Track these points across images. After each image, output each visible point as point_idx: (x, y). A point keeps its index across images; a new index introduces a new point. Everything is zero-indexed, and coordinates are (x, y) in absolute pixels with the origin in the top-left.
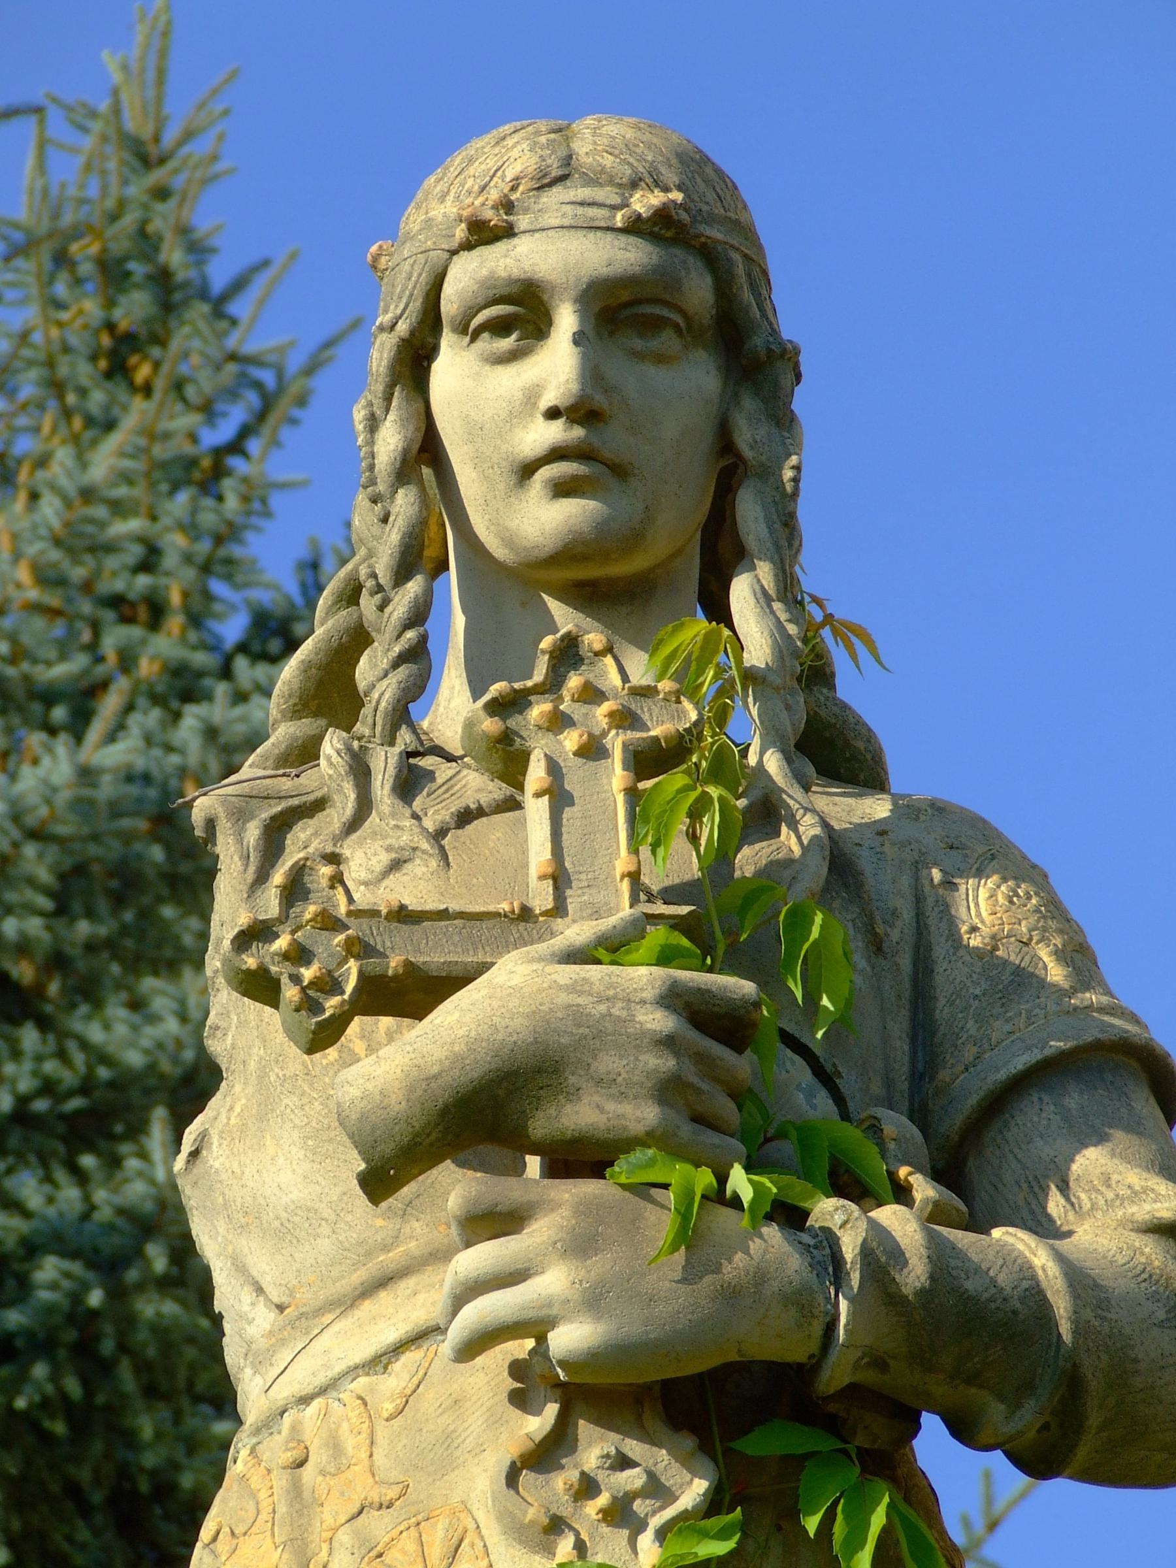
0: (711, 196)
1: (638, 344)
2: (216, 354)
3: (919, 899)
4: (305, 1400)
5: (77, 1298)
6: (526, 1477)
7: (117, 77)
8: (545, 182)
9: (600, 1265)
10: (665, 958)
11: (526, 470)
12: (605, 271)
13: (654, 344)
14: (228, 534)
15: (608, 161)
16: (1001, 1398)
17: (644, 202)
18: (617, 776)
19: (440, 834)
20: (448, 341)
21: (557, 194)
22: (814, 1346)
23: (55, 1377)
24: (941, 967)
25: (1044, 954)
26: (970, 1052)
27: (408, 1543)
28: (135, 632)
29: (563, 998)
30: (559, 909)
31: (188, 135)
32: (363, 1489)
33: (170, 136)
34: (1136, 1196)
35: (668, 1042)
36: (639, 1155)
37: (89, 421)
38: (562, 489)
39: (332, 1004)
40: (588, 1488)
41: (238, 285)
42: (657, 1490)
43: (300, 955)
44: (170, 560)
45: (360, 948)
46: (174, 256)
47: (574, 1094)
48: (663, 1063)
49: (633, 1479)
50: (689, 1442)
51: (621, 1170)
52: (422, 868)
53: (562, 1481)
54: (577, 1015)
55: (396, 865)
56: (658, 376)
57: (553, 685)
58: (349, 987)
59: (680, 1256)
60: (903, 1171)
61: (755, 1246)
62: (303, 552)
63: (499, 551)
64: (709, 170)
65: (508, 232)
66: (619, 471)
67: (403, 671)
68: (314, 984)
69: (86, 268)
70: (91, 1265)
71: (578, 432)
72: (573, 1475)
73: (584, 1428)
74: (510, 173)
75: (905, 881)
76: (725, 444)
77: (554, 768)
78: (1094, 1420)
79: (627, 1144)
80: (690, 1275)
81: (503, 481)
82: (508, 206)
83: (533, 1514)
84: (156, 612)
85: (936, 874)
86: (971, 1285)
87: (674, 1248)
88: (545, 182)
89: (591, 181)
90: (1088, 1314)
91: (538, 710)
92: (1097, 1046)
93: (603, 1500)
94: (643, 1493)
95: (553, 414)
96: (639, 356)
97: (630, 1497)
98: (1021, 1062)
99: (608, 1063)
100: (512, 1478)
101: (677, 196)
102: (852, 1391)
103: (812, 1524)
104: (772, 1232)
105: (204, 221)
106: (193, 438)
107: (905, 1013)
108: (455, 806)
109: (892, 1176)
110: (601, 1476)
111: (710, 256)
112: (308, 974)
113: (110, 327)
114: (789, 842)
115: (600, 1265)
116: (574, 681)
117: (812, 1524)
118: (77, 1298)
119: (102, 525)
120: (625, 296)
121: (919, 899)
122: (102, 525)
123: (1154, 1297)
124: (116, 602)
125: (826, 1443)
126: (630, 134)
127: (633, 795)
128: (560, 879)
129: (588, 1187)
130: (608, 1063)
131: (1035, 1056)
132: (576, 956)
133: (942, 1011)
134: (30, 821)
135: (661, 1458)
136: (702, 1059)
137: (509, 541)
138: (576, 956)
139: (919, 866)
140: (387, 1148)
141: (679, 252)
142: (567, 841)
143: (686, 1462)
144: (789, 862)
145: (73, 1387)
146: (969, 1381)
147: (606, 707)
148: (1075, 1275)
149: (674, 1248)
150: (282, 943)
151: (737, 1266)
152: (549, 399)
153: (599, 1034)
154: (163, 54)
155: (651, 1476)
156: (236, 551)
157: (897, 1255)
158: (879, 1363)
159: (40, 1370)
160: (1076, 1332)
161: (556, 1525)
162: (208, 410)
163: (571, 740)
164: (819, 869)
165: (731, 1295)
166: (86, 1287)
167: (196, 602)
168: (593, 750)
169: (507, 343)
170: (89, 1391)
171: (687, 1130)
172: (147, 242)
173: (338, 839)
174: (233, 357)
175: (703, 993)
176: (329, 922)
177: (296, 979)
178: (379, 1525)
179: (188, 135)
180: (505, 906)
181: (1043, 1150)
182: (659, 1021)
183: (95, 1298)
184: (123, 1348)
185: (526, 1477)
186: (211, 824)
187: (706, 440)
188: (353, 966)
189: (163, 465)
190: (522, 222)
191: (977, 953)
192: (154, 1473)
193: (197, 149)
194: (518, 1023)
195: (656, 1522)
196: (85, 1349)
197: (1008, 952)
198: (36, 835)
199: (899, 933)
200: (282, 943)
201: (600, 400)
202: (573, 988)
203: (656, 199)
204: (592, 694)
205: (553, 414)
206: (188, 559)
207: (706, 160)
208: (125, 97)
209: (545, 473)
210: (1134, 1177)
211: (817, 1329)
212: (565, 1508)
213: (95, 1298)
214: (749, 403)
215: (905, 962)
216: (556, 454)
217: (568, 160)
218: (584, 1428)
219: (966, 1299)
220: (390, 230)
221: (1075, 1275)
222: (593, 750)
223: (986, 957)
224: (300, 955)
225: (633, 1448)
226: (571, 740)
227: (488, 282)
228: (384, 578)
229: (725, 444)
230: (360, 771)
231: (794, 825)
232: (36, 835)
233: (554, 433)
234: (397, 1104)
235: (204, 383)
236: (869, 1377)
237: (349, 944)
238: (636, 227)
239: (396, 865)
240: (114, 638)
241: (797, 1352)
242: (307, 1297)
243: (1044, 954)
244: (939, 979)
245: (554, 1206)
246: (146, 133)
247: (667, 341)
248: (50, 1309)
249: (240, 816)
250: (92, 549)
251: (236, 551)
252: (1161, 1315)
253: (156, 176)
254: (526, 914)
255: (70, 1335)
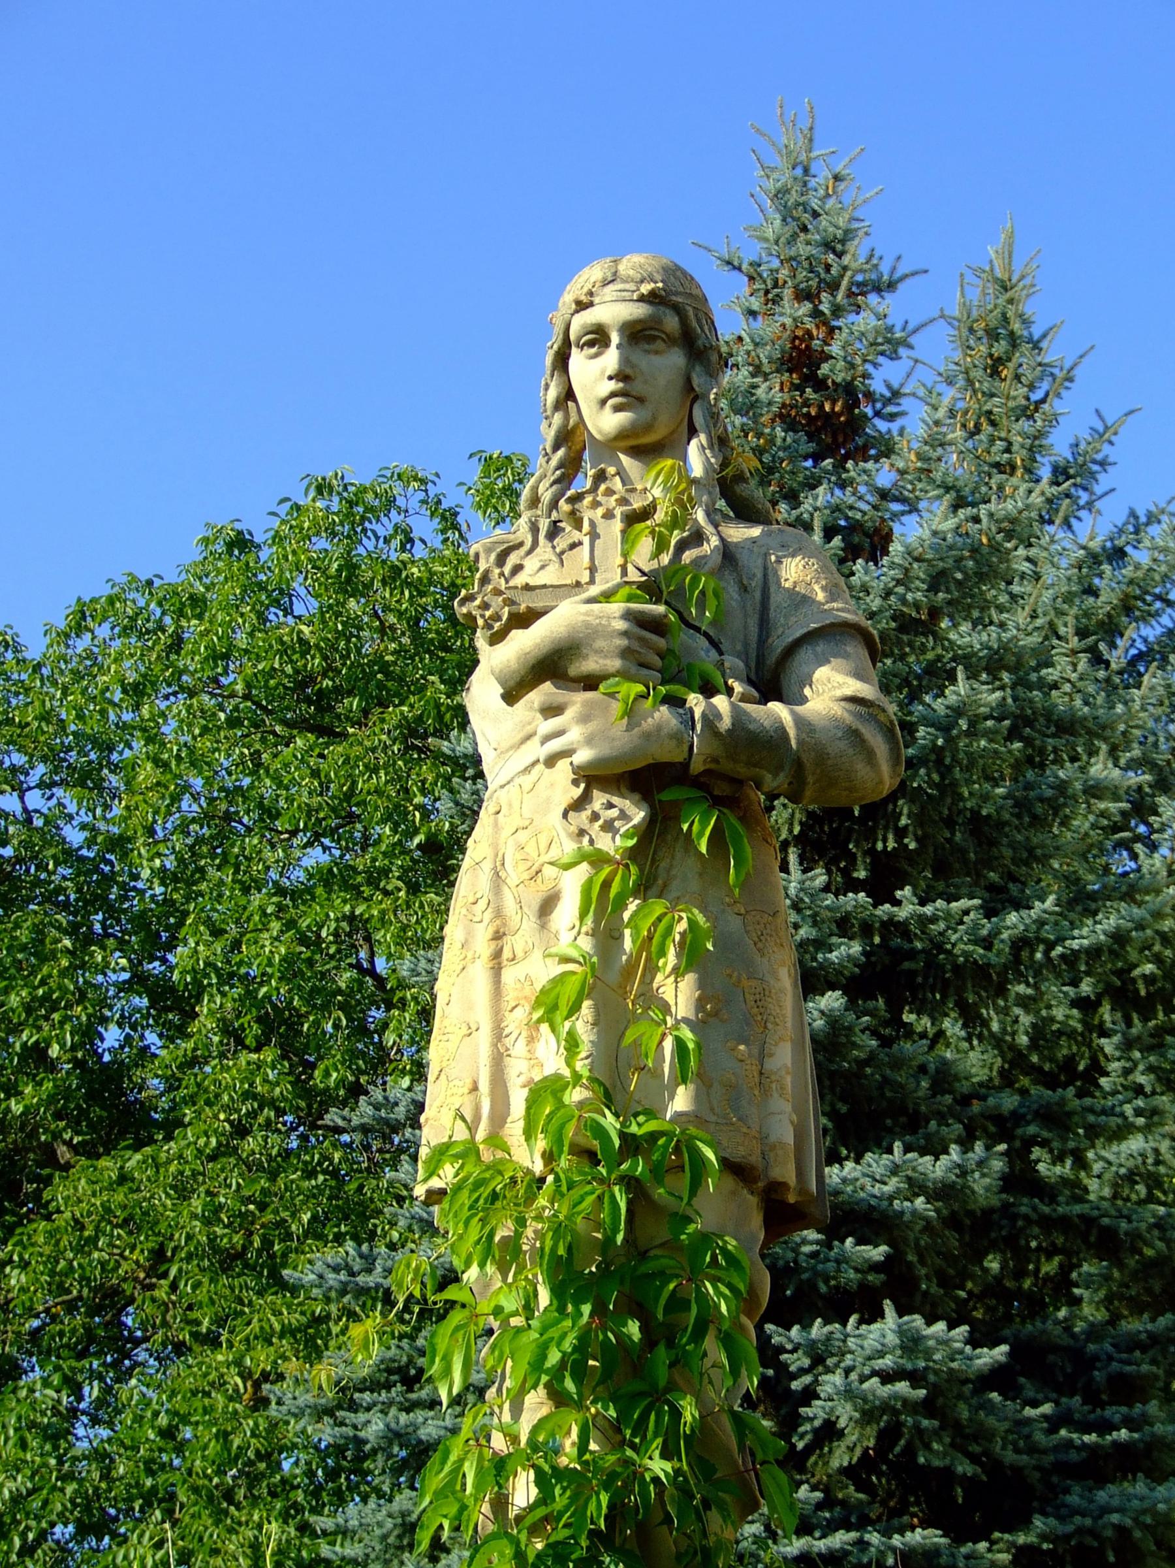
0: (677, 284)
1: (647, 347)
2: (1033, 364)
3: (765, 568)
4: (502, 787)
5: (934, 742)
6: (571, 814)
7: (993, 256)
8: (606, 283)
9: (592, 726)
10: (630, 599)
11: (603, 402)
12: (629, 318)
13: (652, 347)
14: (1040, 435)
15: (631, 272)
16: (769, 772)
17: (645, 288)
18: (617, 525)
19: (563, 553)
20: (574, 351)
21: (611, 287)
22: (686, 755)
23: (928, 775)
24: (773, 595)
25: (817, 587)
26: (780, 631)
27: (533, 842)
28: (1004, 476)
29: (582, 618)
30: (592, 581)
31: (1022, 277)
32: (518, 822)
33: (1014, 280)
34: (840, 686)
35: (625, 634)
36: (612, 681)
37: (984, 393)
38: (617, 409)
39: (497, 626)
40: (595, 817)
41: (1044, 336)
42: (623, 816)
43: (485, 606)
44: (1015, 448)
45: (510, 602)
46: (1016, 326)
47: (586, 657)
48: (623, 642)
49: (614, 813)
50: (637, 797)
51: (602, 688)
52: (553, 567)
53: (586, 814)
54: (587, 625)
55: (542, 567)
56: (656, 360)
57: (594, 489)
58: (505, 618)
59: (625, 721)
60: (730, 681)
61: (657, 715)
62: (1073, 441)
63: (598, 436)
64: (679, 273)
65: (591, 304)
66: (641, 400)
67: (555, 487)
68: (490, 618)
69: (980, 333)
70: (938, 729)
71: (621, 385)
72: (589, 812)
73: (596, 793)
74: (592, 280)
75: (760, 562)
76: (688, 386)
77: (592, 524)
78: (810, 780)
79: (604, 677)
80: (630, 727)
81: (595, 407)
82: (591, 294)
83: (573, 829)
84: (1013, 468)
85: (773, 558)
86: (751, 727)
87: (622, 718)
88: (606, 283)
89: (624, 281)
90: (804, 736)
91: (588, 499)
92: (832, 625)
93: (601, 822)
94: (618, 818)
95: (610, 378)
96: (648, 352)
97: (613, 820)
98: (798, 634)
99: (600, 644)
100: (565, 815)
101: (660, 285)
102: (708, 772)
103: (685, 827)
104: (664, 709)
105: (1028, 308)
106: (1028, 399)
107: (757, 616)
108: (570, 541)
109: (726, 683)
110: (601, 812)
111: (677, 309)
112: (488, 614)
113: (991, 356)
114: (706, 548)
115: (592, 726)
116: (603, 487)
117: (685, 827)
118: (934, 742)
119: (945, 435)
120: (639, 327)
121: (765, 568)
122: (945, 435)
123: (837, 727)
124: (997, 465)
125: (693, 793)
126: (642, 260)
127: (623, 532)
128: (593, 569)
129: (590, 695)
130: (600, 644)
131: (805, 630)
132: (592, 600)
133: (772, 614)
134: (916, 554)
135: (625, 804)
136: (641, 639)
137: (600, 432)
138: (592, 600)
139: (766, 555)
140: (512, 683)
141: (662, 308)
142: (596, 553)
143: (636, 804)
144: (705, 556)
145: (936, 777)
146: (755, 766)
147: (615, 497)
148: (799, 721)
149: (622, 718)
150: (477, 602)
151: (649, 723)
152: (609, 372)
153: (596, 632)
154: (1010, 245)
155: (622, 811)
156: (1044, 442)
157: (719, 716)
158: (715, 760)
159: (922, 771)
160: (799, 743)
161: (582, 833)
162: (1032, 387)
163: (600, 511)
164: (718, 559)
165: (647, 736)
166: (937, 738)
167: (1027, 463)
168: (609, 515)
169: (593, 350)
170: (943, 778)
171: (634, 669)
172: (1005, 319)
173: (522, 558)
174: (1040, 364)
175: (641, 613)
176: (497, 592)
177: (483, 616)
178: (522, 836)
179: (1022, 277)
180: (568, 582)
181: (805, 669)
182: (621, 625)
183: (940, 742)
184: (954, 758)
185: (571, 814)
186: (477, 555)
187: (680, 382)
188: (506, 609)
189: (1012, 409)
190: (596, 300)
191: (787, 590)
192: (972, 810)
193: (1028, 281)
194: (562, 629)
195: (622, 830)
196: (939, 762)
197: (800, 589)
198: (918, 559)
199: (756, 583)
200: (477, 602)
201: (629, 371)
202: (587, 614)
203: (651, 286)
204: (610, 492)
205: (610, 378)
206: (1022, 446)
207: (678, 268)
208: (996, 263)
209: (611, 402)
210: (840, 678)
211: (686, 748)
212: (586, 825)
213: (940, 742)
214: (698, 368)
215: (758, 595)
216: (613, 395)
217: (615, 274)
218: (596, 793)
219: (749, 732)
220: (556, 309)
221: (799, 721)
222: (609, 515)
223: (791, 592)
224: (485, 606)
225: (615, 800)
226: (600, 511)
227: (584, 326)
228: (549, 450)
229: (688, 386)
230: (534, 529)
231: (708, 541)
232: (918, 559)
233: (613, 386)
234: (514, 665)
235: (1028, 375)
236: (713, 766)
237: (504, 601)
238: (642, 299)
239: (542, 567)
240: (997, 478)
241: (679, 757)
242: (505, 745)
243: (817, 587)
244: (772, 600)
245: (574, 703)
246: (1006, 277)
247: (659, 345)
248: (924, 747)
249: (489, 551)
250: (942, 445)
251: (1044, 442)
252: (840, 734)
253: (1009, 294)
254: (578, 584)
255: (933, 757)
